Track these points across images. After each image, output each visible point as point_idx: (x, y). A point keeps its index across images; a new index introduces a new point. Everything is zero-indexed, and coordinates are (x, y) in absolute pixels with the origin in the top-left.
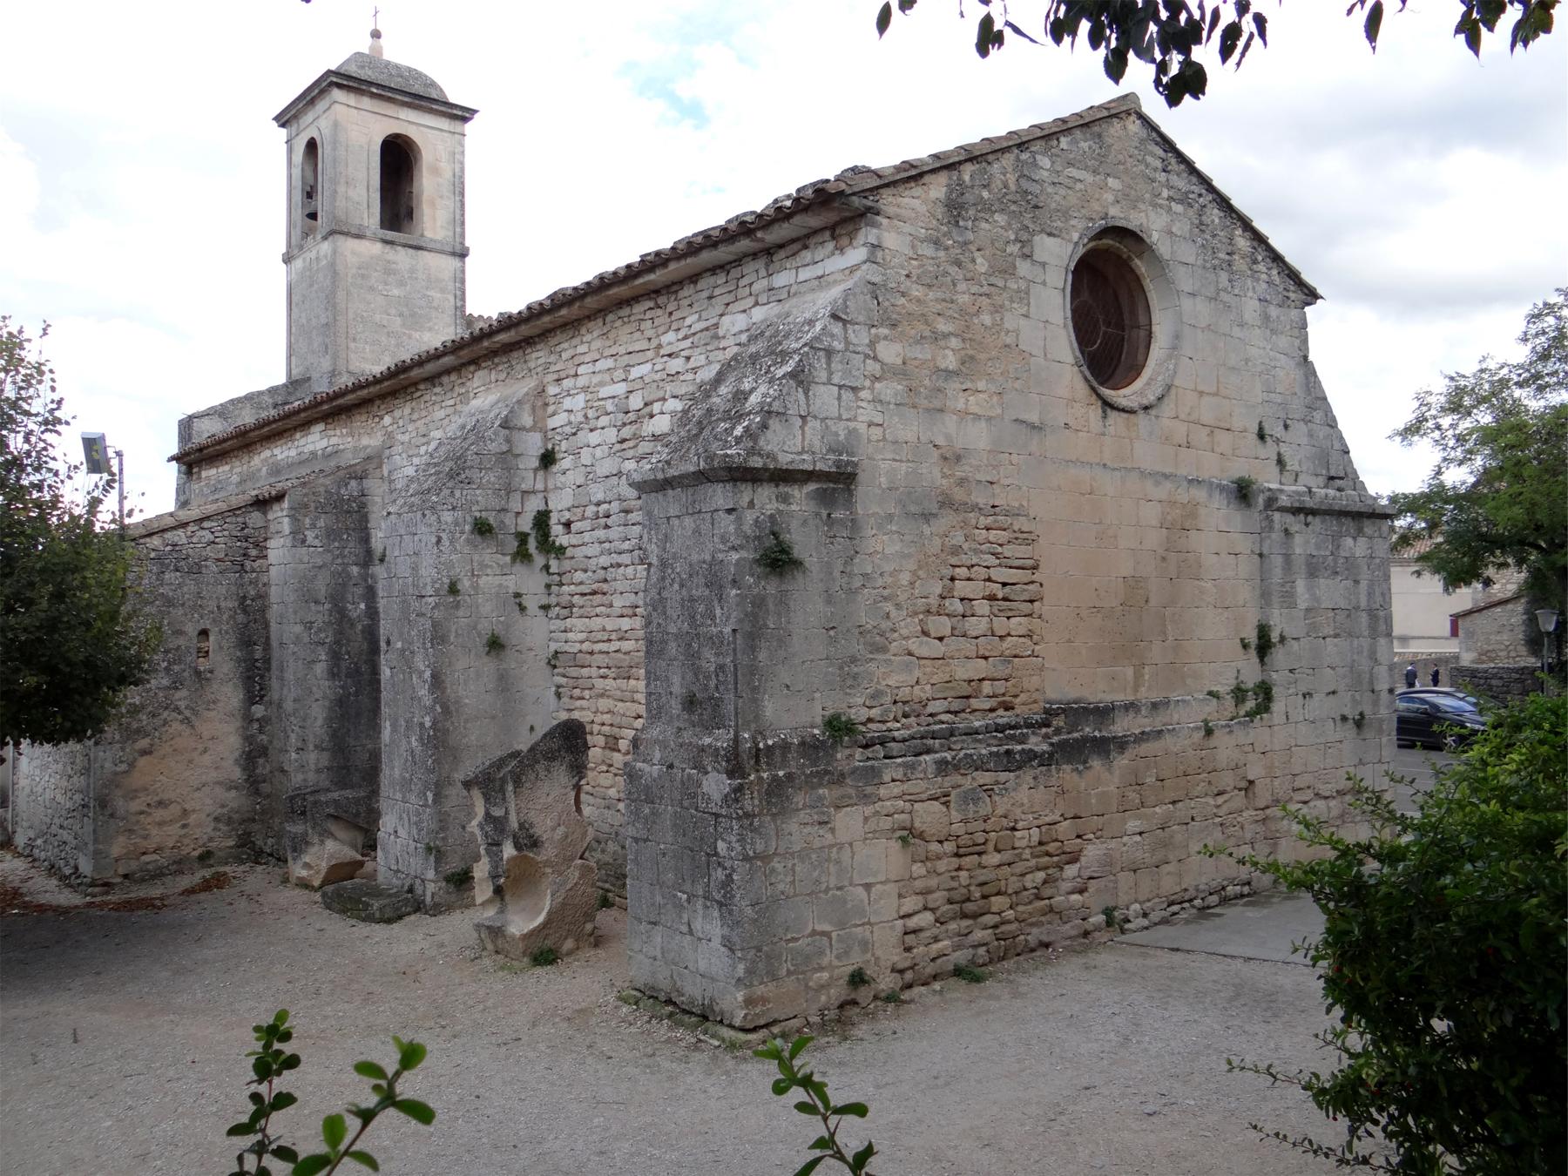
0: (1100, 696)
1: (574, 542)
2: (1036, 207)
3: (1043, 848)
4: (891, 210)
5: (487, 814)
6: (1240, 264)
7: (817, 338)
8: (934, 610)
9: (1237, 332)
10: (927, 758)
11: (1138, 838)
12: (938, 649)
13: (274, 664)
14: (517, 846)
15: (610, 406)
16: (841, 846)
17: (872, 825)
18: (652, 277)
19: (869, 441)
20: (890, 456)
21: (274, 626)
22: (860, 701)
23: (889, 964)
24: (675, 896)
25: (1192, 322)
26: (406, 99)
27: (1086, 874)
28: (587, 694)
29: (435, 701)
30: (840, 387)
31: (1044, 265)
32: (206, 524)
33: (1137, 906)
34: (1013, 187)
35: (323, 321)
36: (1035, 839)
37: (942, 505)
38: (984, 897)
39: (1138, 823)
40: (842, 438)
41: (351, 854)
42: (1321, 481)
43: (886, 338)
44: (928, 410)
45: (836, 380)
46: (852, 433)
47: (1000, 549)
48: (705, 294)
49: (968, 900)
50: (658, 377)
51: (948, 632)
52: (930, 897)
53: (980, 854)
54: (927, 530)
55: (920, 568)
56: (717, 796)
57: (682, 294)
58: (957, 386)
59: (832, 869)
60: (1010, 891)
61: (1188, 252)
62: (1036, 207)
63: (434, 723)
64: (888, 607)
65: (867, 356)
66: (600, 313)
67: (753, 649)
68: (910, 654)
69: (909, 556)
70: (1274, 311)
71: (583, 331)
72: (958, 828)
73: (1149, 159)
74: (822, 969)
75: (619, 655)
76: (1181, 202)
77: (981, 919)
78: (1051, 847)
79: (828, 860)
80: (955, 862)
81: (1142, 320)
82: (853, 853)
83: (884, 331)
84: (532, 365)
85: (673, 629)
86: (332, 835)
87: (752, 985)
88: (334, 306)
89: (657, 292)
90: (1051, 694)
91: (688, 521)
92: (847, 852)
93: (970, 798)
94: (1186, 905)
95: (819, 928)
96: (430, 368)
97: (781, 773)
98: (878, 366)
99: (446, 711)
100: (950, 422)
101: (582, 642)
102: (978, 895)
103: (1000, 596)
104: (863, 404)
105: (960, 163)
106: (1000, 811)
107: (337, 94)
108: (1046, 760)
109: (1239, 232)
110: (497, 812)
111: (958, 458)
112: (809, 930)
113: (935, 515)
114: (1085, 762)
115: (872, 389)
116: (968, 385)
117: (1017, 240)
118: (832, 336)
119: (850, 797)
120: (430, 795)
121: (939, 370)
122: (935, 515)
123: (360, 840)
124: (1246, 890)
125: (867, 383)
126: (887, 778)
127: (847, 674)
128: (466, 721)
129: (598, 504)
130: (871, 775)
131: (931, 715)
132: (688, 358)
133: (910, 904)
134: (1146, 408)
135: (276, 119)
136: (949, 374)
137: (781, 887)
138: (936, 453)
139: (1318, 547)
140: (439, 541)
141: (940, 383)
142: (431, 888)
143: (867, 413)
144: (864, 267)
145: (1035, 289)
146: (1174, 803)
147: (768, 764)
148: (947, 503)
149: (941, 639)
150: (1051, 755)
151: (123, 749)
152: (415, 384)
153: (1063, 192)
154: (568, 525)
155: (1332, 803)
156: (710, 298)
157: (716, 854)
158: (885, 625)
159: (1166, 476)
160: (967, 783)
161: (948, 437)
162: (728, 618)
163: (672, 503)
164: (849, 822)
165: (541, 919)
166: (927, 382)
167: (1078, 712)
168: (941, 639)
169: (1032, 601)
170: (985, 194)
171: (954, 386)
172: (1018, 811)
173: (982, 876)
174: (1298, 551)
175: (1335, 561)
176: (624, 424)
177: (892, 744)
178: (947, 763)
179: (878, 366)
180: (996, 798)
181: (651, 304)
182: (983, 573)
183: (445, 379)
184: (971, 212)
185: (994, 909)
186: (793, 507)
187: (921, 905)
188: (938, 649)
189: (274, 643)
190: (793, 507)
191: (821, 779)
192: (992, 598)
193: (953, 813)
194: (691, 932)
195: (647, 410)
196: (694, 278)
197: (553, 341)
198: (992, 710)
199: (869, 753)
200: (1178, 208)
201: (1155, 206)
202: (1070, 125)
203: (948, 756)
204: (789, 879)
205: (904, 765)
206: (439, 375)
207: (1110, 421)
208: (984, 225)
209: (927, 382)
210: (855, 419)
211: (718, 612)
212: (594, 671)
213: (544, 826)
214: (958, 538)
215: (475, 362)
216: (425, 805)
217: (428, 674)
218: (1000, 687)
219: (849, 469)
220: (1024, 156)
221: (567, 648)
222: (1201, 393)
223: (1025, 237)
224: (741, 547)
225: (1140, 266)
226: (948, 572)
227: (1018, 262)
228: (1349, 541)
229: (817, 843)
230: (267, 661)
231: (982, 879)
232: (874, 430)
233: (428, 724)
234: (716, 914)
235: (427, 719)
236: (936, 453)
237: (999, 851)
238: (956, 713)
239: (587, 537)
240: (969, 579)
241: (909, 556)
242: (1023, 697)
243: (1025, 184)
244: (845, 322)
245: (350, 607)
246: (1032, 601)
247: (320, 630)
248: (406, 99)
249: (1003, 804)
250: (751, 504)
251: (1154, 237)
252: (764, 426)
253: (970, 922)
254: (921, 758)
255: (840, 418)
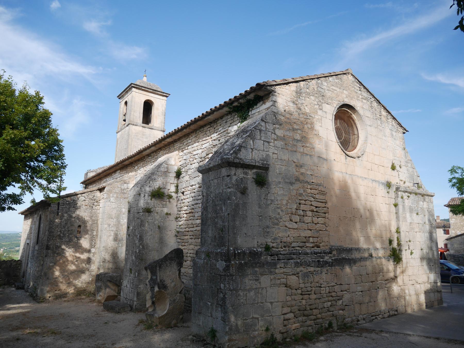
0: (347, 246)
1: (185, 198)
2: (323, 96)
3: (330, 294)
4: (279, 92)
5: (151, 278)
6: (383, 119)
7: (256, 126)
8: (294, 213)
9: (384, 138)
10: (292, 261)
11: (361, 293)
12: (295, 226)
13: (99, 236)
14: (159, 288)
15: (196, 157)
16: (263, 288)
17: (273, 282)
18: (209, 117)
19: (273, 158)
20: (280, 164)
21: (100, 226)
22: (270, 240)
23: (279, 330)
24: (207, 303)
25: (371, 133)
26: (151, 91)
27: (344, 304)
28: (186, 244)
29: (140, 244)
30: (264, 141)
31: (326, 112)
32: (83, 195)
33: (361, 316)
34: (316, 90)
35: (125, 147)
36: (327, 291)
37: (296, 180)
38: (311, 309)
39: (360, 288)
40: (264, 156)
41: (113, 293)
42: (412, 184)
43: (278, 128)
44: (291, 151)
45: (262, 139)
46: (268, 155)
47: (315, 196)
48: (225, 121)
49: (306, 310)
50: (210, 147)
51: (298, 221)
52: (292, 308)
53: (309, 294)
54: (292, 188)
55: (289, 199)
56: (221, 269)
57: (218, 122)
58: (300, 145)
59: (259, 296)
60: (319, 308)
61: (368, 114)
62: (323, 96)
63: (139, 251)
64: (279, 211)
65: (272, 133)
66: (195, 131)
67: (234, 220)
68: (286, 227)
69: (286, 195)
70: (394, 134)
71: (190, 136)
72: (302, 285)
73: (355, 87)
74: (255, 331)
75: (196, 231)
76: (365, 99)
77: (310, 317)
78: (333, 294)
79: (258, 293)
80: (301, 297)
81: (356, 133)
82: (267, 291)
83: (277, 126)
84: (175, 147)
85: (210, 216)
86: (109, 287)
87: (231, 334)
88: (128, 143)
89: (211, 123)
90: (332, 244)
91: (216, 181)
92: (264, 291)
93: (306, 275)
94: (377, 317)
95: (255, 316)
96: (148, 151)
97: (243, 262)
98: (276, 136)
99: (143, 247)
100: (299, 155)
101: (185, 228)
102: (309, 309)
103: (315, 210)
104: (271, 147)
105: (300, 81)
106: (316, 280)
107: (133, 89)
108: (331, 265)
109: (383, 110)
110: (154, 277)
111: (301, 166)
112: (251, 316)
113: (294, 183)
114: (343, 266)
115: (274, 143)
116: (304, 145)
117: (318, 104)
118: (261, 126)
119: (266, 272)
120: (137, 274)
121: (295, 139)
122: (294, 183)
123: (117, 290)
124: (396, 313)
125: (272, 141)
126: (278, 266)
127: (266, 232)
128: (149, 251)
129: (192, 186)
130: (274, 265)
131: (293, 247)
132: (219, 140)
133: (286, 310)
134: (358, 157)
135: (118, 97)
136: (298, 141)
137: (242, 301)
138: (294, 164)
139: (412, 204)
140: (145, 195)
141: (295, 143)
142: (135, 303)
143: (272, 150)
144: (271, 107)
145: (323, 119)
146: (372, 282)
147: (238, 258)
148: (297, 180)
149: (296, 223)
150: (332, 263)
151: (53, 259)
152: (144, 157)
153: (331, 93)
154: (183, 193)
155: (422, 286)
156: (226, 122)
157: (221, 289)
158: (278, 216)
159: (366, 178)
160: (305, 270)
161: (297, 159)
162: (227, 210)
163: (212, 175)
164: (265, 280)
165: (165, 312)
166: (291, 142)
167: (341, 250)
168: (296, 223)
169: (325, 213)
170: (308, 90)
171: (300, 144)
172: (322, 281)
173: (312, 302)
174: (406, 204)
175: (418, 208)
176: (200, 162)
177: (280, 255)
178: (298, 263)
179: (276, 136)
180: (315, 276)
181: (209, 126)
182: (310, 203)
183: (152, 154)
184: (304, 95)
185: (314, 314)
186: (249, 177)
187: (289, 311)
188: (295, 226)
189: (99, 230)
190: (249, 177)
191: (256, 265)
192: (312, 211)
193: (300, 280)
194: (212, 317)
195: (207, 156)
196: (221, 117)
197: (181, 140)
198: (313, 247)
199: (272, 258)
200: (365, 101)
201: (358, 100)
202: (332, 74)
203: (299, 261)
204: (245, 298)
205: (284, 262)
206: (151, 153)
207: (347, 160)
208: (307, 99)
209: (291, 142)
210: (268, 151)
211: (224, 208)
212: (188, 237)
213: (168, 282)
214: (302, 191)
215: (160, 149)
216: (135, 277)
217: (138, 236)
218: (315, 240)
219: (267, 166)
220: (319, 81)
221: (181, 230)
222: (375, 155)
223: (320, 104)
224: (232, 187)
225: (354, 116)
226: (298, 201)
227: (318, 111)
228: (421, 203)
229: (254, 287)
230: (97, 235)
231: (310, 303)
232: (274, 155)
233: (137, 252)
234: (220, 309)
235: (137, 250)
236: (294, 164)
237: (316, 294)
238: (301, 247)
239: (188, 196)
240: (305, 204)
241: (286, 195)
242: (323, 244)
243: (319, 89)
244: (265, 122)
245: (121, 220)
246: (325, 213)
247: (112, 227)
248: (151, 91)
249: (317, 278)
250: (235, 174)
251: (358, 108)
252: (240, 150)
253: (306, 318)
254: (290, 261)
255: (264, 150)
